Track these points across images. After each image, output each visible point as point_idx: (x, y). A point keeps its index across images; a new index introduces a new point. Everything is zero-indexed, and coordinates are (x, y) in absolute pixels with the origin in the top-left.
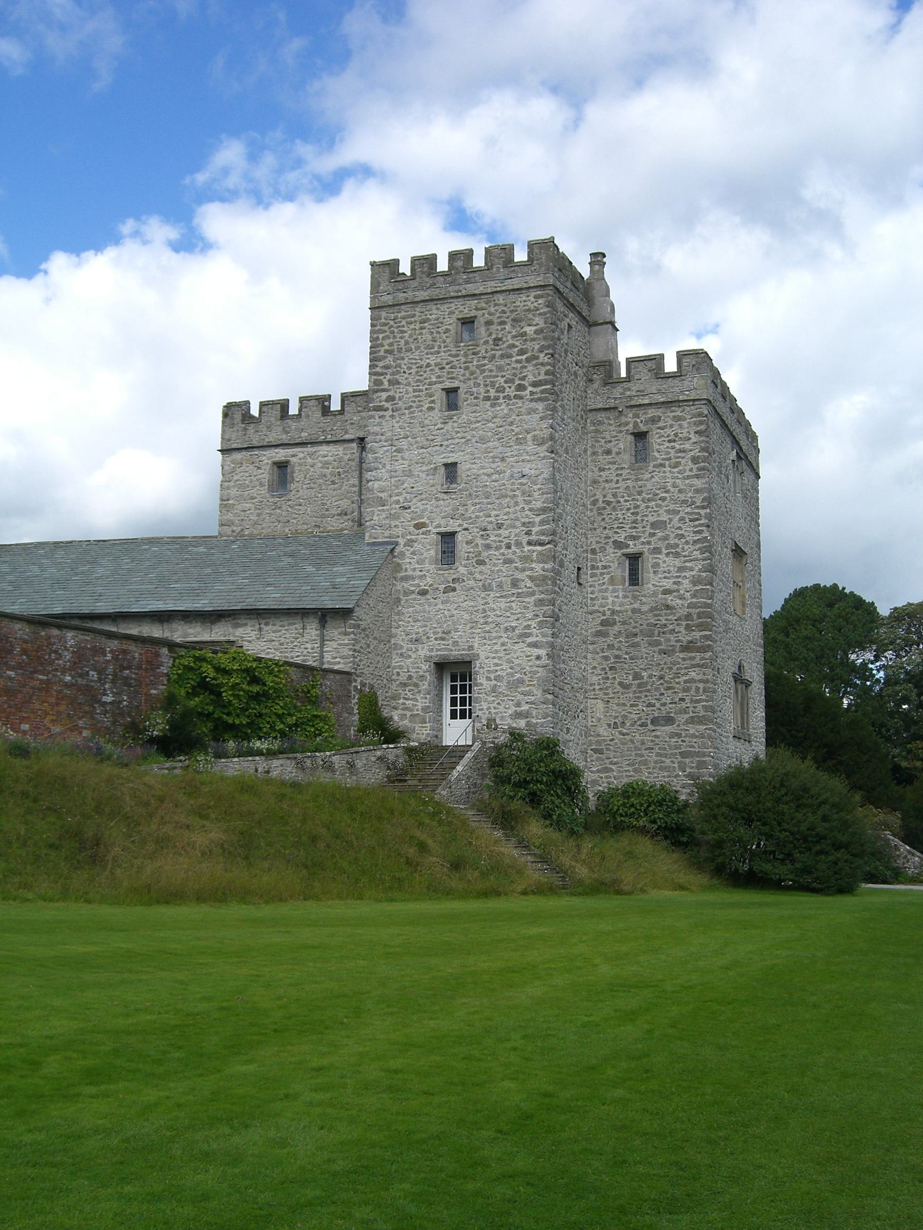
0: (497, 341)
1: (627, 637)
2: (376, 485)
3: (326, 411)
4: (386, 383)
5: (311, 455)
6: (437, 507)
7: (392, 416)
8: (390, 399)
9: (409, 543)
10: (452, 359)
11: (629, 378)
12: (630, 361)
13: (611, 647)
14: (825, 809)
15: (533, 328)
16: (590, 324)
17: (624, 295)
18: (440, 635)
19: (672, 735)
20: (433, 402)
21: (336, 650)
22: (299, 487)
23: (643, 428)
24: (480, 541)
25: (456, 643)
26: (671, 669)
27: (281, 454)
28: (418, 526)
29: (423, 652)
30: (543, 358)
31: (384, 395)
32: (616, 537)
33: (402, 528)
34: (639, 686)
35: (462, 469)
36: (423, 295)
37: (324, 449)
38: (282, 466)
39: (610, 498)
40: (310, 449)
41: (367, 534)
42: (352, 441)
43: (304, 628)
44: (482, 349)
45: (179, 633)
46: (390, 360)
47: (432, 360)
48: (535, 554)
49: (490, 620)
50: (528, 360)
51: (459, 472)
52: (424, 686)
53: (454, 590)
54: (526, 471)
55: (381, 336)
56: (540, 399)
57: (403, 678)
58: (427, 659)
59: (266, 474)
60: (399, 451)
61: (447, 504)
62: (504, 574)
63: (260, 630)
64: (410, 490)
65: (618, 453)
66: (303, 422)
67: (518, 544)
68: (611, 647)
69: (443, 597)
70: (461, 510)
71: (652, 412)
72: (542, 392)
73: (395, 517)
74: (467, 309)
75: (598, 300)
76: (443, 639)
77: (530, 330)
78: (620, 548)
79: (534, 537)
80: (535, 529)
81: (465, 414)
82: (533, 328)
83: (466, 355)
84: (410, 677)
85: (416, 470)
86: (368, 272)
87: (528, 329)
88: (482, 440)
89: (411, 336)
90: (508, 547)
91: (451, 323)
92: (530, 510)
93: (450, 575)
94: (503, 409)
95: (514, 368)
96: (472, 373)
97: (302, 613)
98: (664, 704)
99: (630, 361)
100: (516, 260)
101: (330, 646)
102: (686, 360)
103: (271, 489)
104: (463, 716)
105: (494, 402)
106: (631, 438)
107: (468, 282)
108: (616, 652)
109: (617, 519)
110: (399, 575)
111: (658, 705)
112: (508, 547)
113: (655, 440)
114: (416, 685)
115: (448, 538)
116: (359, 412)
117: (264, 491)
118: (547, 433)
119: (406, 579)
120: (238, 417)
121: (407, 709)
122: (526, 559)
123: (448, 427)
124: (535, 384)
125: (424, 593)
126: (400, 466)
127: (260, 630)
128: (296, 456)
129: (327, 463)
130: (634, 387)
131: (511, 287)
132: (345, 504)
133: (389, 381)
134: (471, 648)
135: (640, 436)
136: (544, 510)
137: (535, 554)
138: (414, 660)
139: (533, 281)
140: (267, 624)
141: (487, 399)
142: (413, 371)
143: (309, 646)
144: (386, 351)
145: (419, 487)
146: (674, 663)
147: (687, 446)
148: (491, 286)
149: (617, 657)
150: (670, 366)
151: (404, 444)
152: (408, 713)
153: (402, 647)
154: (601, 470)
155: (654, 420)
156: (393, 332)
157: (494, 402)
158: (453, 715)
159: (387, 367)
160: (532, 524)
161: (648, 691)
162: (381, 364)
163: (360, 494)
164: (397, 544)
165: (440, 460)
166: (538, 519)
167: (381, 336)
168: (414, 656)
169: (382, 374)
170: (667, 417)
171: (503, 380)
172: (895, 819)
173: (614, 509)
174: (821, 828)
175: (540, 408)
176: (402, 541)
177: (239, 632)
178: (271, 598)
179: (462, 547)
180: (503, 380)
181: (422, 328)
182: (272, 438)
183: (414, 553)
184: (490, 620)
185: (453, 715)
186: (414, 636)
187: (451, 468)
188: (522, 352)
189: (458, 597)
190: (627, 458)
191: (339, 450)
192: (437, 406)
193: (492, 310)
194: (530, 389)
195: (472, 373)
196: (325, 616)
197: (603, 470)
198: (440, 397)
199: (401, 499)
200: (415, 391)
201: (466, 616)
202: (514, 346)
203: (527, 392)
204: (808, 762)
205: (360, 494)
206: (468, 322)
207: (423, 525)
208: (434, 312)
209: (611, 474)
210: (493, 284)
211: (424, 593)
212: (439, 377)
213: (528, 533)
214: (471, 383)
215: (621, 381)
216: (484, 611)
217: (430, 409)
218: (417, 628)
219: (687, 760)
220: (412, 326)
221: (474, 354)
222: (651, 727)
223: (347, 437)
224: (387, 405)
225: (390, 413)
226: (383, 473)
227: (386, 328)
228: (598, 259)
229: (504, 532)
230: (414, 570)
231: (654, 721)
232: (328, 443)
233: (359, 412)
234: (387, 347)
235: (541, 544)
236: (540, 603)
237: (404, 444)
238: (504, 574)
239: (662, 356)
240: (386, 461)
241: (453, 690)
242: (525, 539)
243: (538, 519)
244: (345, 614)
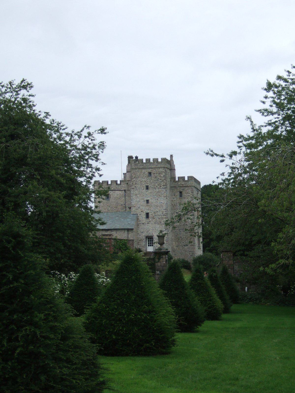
0: (156, 177)
1: (179, 230)
2: (133, 203)
3: (117, 184)
4: (134, 184)
5: (114, 193)
6: (145, 208)
7: (136, 190)
8: (135, 187)
9: (140, 214)
10: (147, 180)
12: (178, 178)
13: (176, 232)
15: (163, 175)
18: (147, 231)
19: (188, 248)
20: (144, 188)
21: (131, 236)
23: (181, 191)
24: (154, 215)
25: (150, 233)
26: (187, 236)
28: (142, 211)
29: (144, 234)
31: (134, 186)
32: (176, 211)
33: (138, 212)
34: (181, 239)
35: (150, 201)
37: (117, 192)
39: (175, 204)
40: (114, 191)
41: (132, 212)
42: (123, 190)
43: (125, 232)
44: (153, 178)
45: (101, 233)
47: (143, 180)
48: (164, 217)
49: (156, 229)
50: (162, 181)
51: (149, 202)
52: (144, 241)
53: (149, 223)
54: (162, 202)
55: (133, 174)
56: (164, 189)
57: (140, 239)
58: (145, 236)
60: (137, 197)
61: (147, 208)
63: (116, 232)
64: (140, 205)
65: (177, 195)
67: (161, 215)
68: (176, 232)
69: (147, 225)
70: (150, 209)
71: (183, 188)
72: (165, 187)
73: (137, 209)
74: (150, 170)
76: (147, 232)
78: (177, 213)
79: (164, 214)
80: (164, 213)
82: (163, 175)
83: (150, 179)
84: (141, 239)
86: (127, 158)
87: (161, 175)
89: (139, 175)
90: (159, 216)
91: (147, 173)
92: (163, 209)
95: (159, 183)
96: (151, 183)
97: (124, 229)
98: (186, 243)
99: (178, 178)
100: (159, 161)
101: (130, 235)
102: (189, 178)
104: (151, 246)
105: (155, 189)
106: (179, 193)
107: (150, 165)
108: (177, 233)
109: (177, 208)
110: (138, 220)
111: (185, 243)
112: (159, 216)
114: (142, 241)
116: (124, 184)
119: (140, 221)
121: (141, 245)
123: (147, 193)
124: (163, 186)
125: (143, 224)
126: (138, 200)
127: (116, 232)
129: (118, 194)
131: (158, 167)
132: (122, 203)
133: (135, 183)
134: (153, 234)
136: (165, 209)
137: (164, 217)
138: (143, 236)
139: (162, 166)
140: (117, 231)
141: (154, 188)
142: (140, 182)
143: (126, 235)
144: (134, 177)
145: (142, 204)
146: (188, 235)
147: (189, 195)
149: (177, 234)
150: (186, 179)
152: (141, 246)
153: (139, 234)
154: (173, 198)
156: (135, 174)
157: (155, 189)
158: (149, 246)
159: (134, 181)
160: (163, 212)
161: (183, 240)
162: (133, 180)
163: (125, 201)
164: (138, 214)
165: (146, 199)
166: (164, 211)
167: (133, 174)
168: (142, 235)
169: (133, 182)
171: (157, 185)
173: (176, 206)
175: (164, 190)
176: (139, 214)
177: (112, 233)
178: (118, 227)
179: (150, 215)
180: (157, 185)
181: (141, 174)
183: (141, 216)
184: (156, 229)
185: (149, 246)
186: (142, 232)
187: (148, 201)
188: (160, 180)
189: (150, 224)
190: (178, 196)
191: (120, 192)
192: (145, 189)
193: (155, 171)
194: (162, 187)
195: (151, 183)
196: (128, 230)
197: (174, 198)
198: (145, 187)
199: (138, 206)
200: (140, 186)
201: (152, 228)
202: (159, 178)
203: (162, 187)
205: (125, 201)
206: (150, 173)
207: (143, 211)
208: (143, 171)
209: (175, 199)
210: (154, 166)
211: (143, 224)
212: (145, 183)
213: (163, 213)
214: (151, 185)
215: (177, 181)
216: (155, 227)
217: (143, 189)
218: (142, 230)
219: (190, 253)
220: (139, 173)
221: (151, 179)
222: (184, 247)
223: (122, 189)
224: (134, 188)
225: (135, 189)
226: (134, 201)
227: (134, 173)
228: (171, 156)
229: (158, 213)
230: (141, 219)
231: (184, 246)
232: (118, 190)
233: (124, 184)
234: (134, 177)
235: (165, 215)
239: (185, 177)
241: (149, 241)
242: (162, 214)
243: (164, 211)
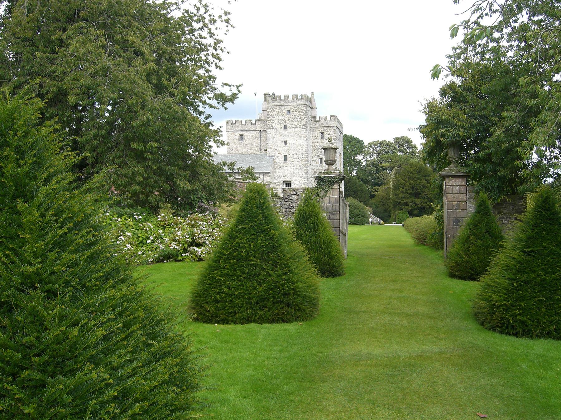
9: (277, 157)
11: (320, 120)
14: (360, 209)
16: (311, 108)
17: (318, 102)
22: (246, 140)
27: (241, 133)
29: (281, 179)
30: (305, 120)
36: (279, 104)
38: (241, 135)
46: (271, 118)
47: (281, 118)
59: (238, 137)
61: (285, 149)
62: (298, 164)
66: (246, 126)
71: (325, 128)
74: (288, 108)
75: (313, 103)
77: (302, 114)
81: (288, 130)
85: (278, 142)
88: (292, 136)
91: (285, 111)
93: (286, 163)
94: (296, 130)
103: (239, 141)
113: (325, 134)
115: (285, 157)
117: (238, 141)
118: (306, 135)
120: (230, 124)
122: (302, 161)
128: (245, 133)
130: (321, 123)
132: (257, 145)
135: (322, 133)
148: (293, 103)
151: (275, 136)
155: (325, 130)
165: (283, 140)
170: (328, 129)
172: (371, 209)
174: (359, 213)
182: (239, 129)
187: (286, 142)
189: (288, 168)
190: (320, 138)
198: (283, 127)
204: (356, 200)
206: (289, 111)
208: (281, 108)
236: (305, 170)
237: (275, 136)
238: (298, 164)
240: (271, 139)
244: (268, 173)
